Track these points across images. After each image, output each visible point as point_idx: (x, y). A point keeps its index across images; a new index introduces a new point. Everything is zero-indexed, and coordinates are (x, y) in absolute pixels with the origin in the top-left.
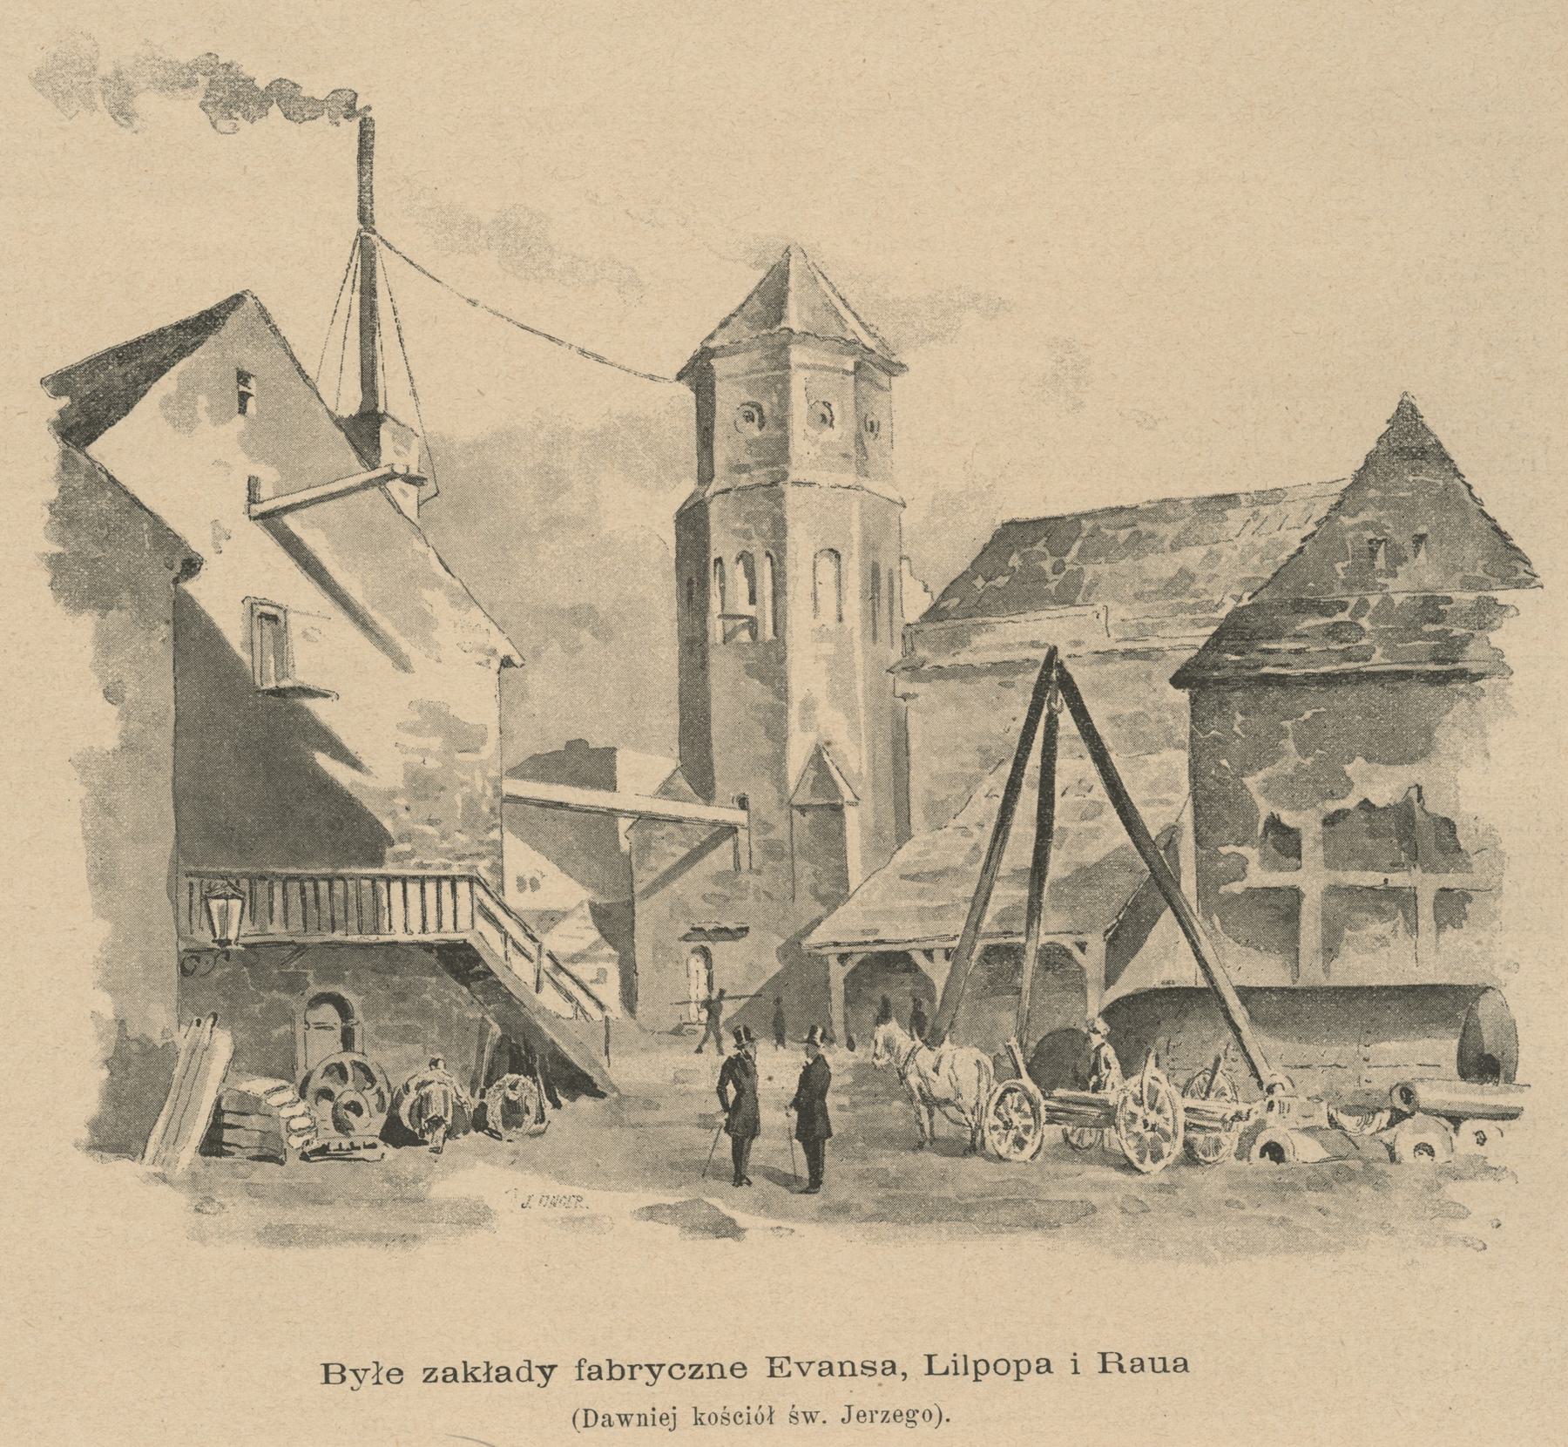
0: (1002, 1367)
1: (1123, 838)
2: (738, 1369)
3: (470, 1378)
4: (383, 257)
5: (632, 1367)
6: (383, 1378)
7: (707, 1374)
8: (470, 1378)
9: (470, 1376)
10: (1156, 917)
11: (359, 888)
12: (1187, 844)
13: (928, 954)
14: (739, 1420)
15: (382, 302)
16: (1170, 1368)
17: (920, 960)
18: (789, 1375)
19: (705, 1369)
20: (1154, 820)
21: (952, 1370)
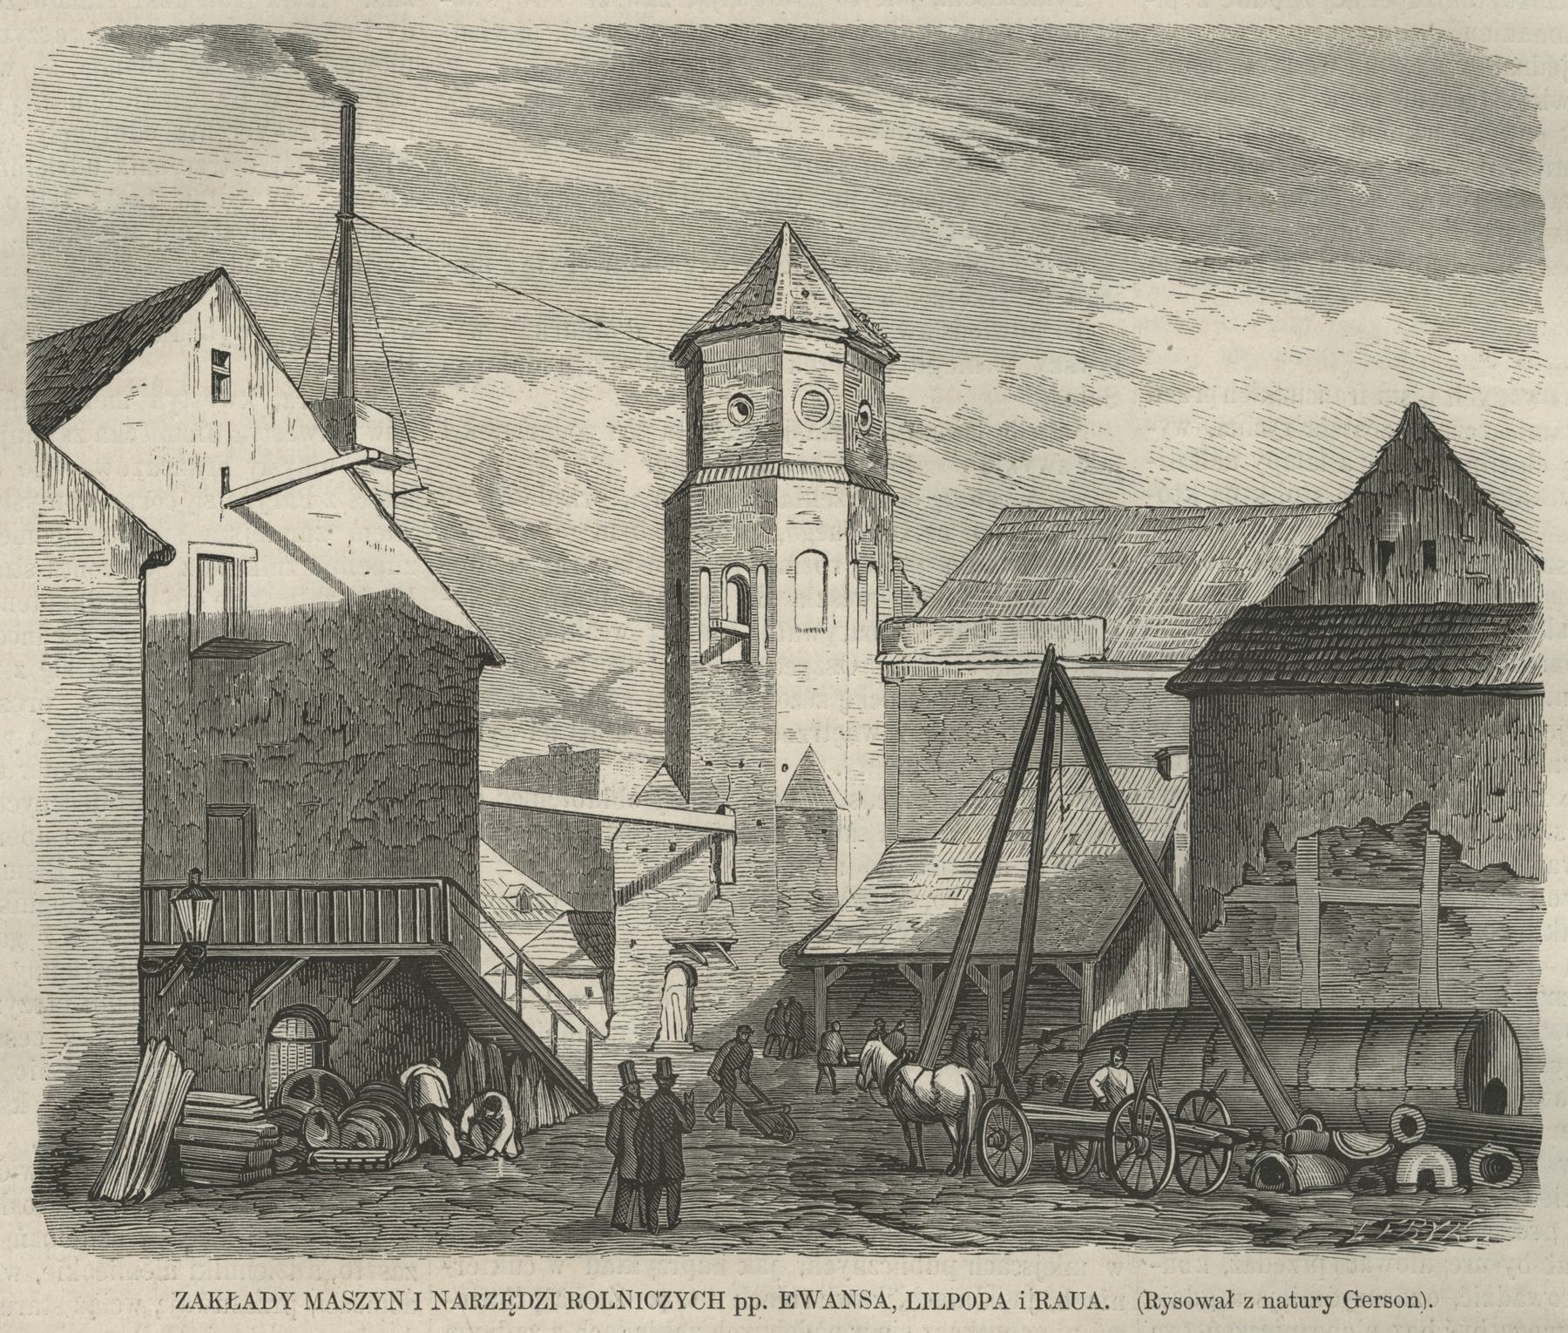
0: (1399, 1302)
1: (1110, 842)
2: (314, 1302)
3: (215, 1305)
4: (361, 231)
5: (1314, 1298)
6: (643, 1304)
7: (500, 1306)
8: (215, 1305)
9: (214, 1303)
10: (776, 487)
11: (343, 902)
12: (1181, 858)
13: (917, 968)
14: (1367, 1304)
15: (358, 281)
16: (1373, 1300)
17: (910, 975)
18: (792, 1307)
19: (499, 1299)
20: (1152, 834)
21: (922, 1306)
